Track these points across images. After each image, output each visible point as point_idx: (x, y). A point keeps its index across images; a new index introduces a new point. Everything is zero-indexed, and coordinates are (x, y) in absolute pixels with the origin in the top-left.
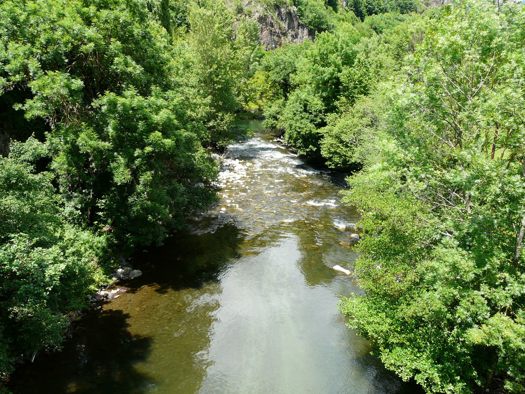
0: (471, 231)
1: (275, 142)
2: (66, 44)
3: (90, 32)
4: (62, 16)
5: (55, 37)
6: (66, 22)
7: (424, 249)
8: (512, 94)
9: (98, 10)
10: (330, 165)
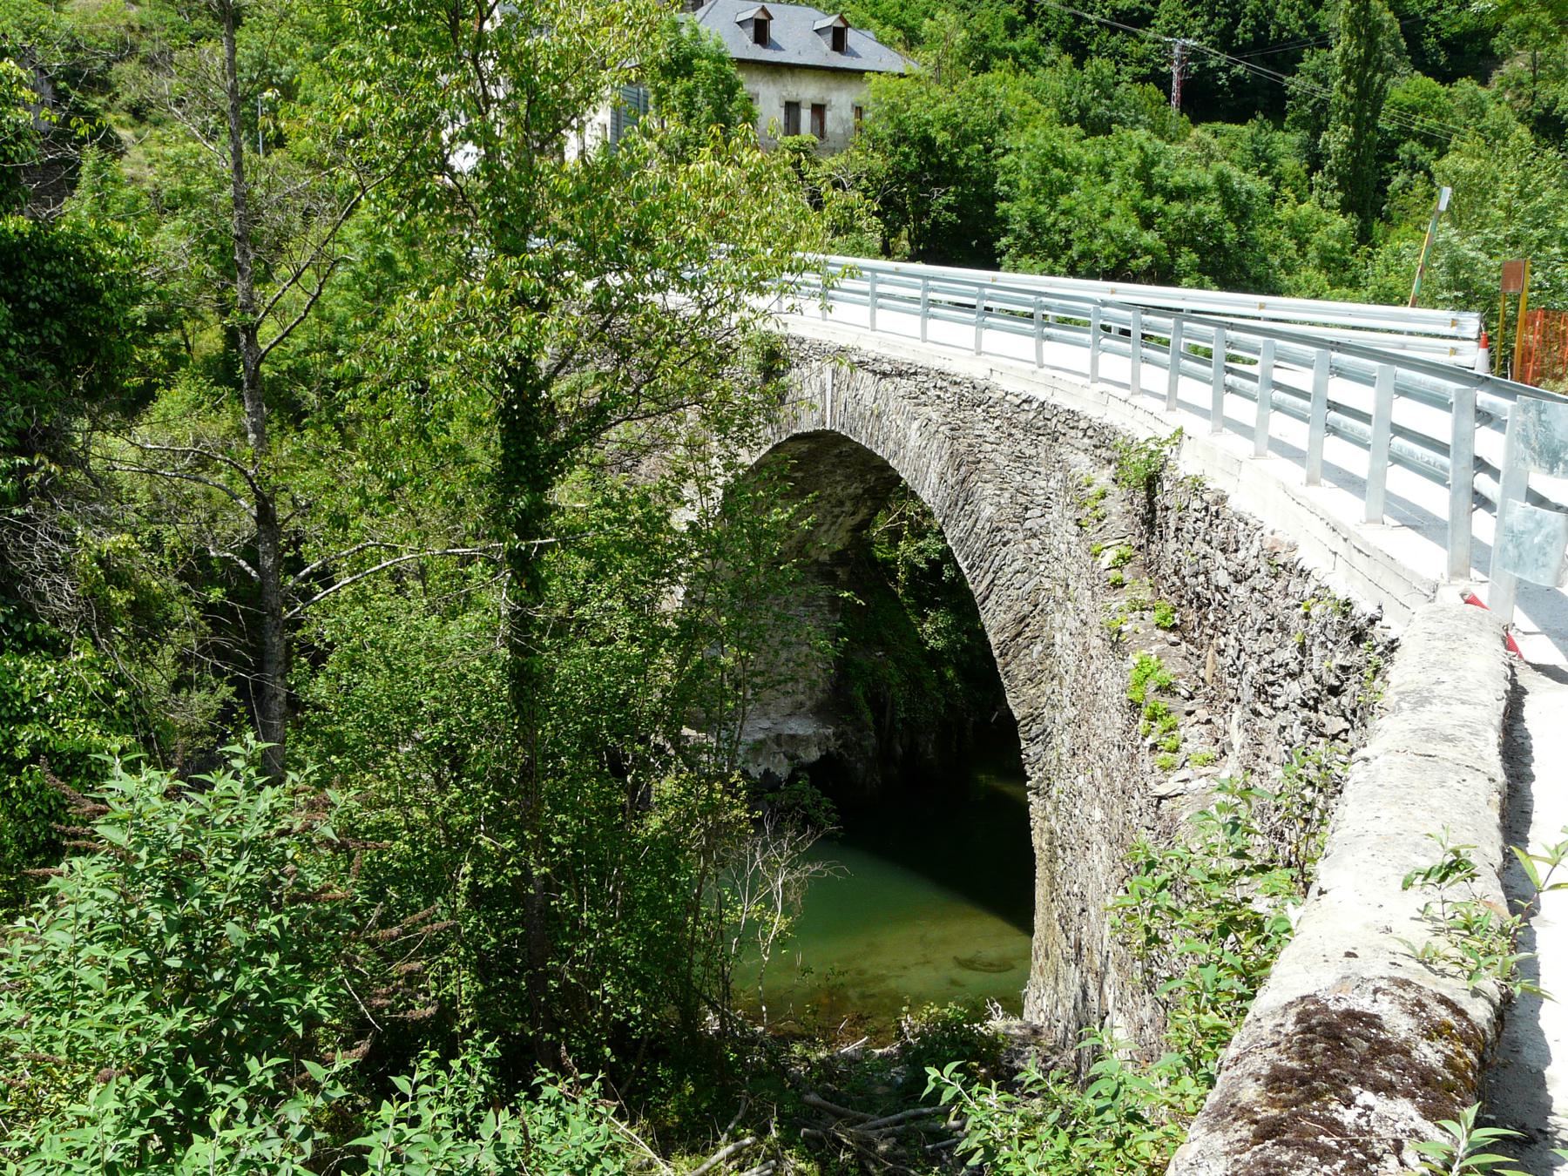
0: (242, 882)
1: (258, 572)
2: (1107, 259)
3: (1149, 238)
4: (1107, 214)
5: (1094, 247)
6: (1113, 224)
7: (296, 548)
8: (243, 56)
9: (1167, 203)
10: (58, 334)
